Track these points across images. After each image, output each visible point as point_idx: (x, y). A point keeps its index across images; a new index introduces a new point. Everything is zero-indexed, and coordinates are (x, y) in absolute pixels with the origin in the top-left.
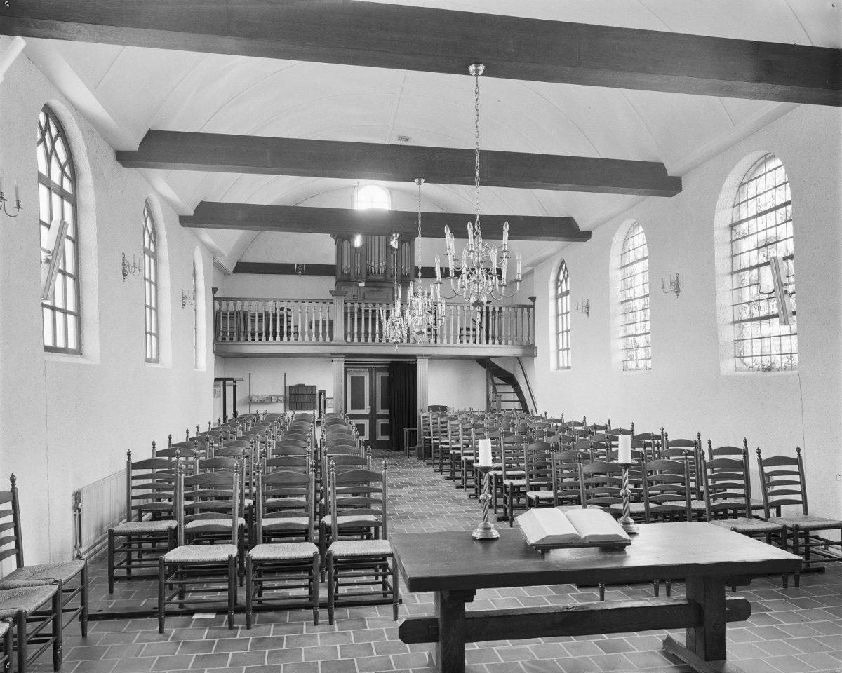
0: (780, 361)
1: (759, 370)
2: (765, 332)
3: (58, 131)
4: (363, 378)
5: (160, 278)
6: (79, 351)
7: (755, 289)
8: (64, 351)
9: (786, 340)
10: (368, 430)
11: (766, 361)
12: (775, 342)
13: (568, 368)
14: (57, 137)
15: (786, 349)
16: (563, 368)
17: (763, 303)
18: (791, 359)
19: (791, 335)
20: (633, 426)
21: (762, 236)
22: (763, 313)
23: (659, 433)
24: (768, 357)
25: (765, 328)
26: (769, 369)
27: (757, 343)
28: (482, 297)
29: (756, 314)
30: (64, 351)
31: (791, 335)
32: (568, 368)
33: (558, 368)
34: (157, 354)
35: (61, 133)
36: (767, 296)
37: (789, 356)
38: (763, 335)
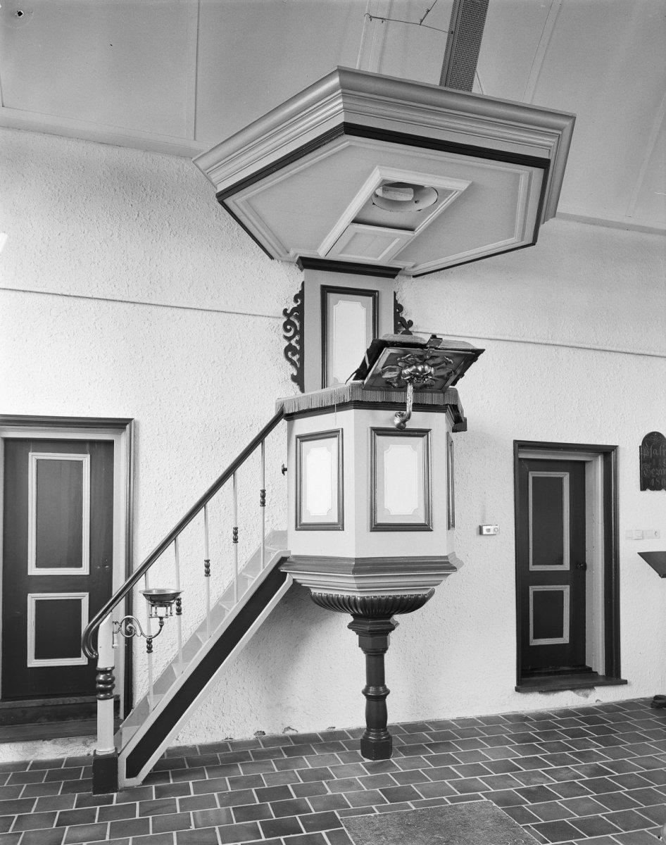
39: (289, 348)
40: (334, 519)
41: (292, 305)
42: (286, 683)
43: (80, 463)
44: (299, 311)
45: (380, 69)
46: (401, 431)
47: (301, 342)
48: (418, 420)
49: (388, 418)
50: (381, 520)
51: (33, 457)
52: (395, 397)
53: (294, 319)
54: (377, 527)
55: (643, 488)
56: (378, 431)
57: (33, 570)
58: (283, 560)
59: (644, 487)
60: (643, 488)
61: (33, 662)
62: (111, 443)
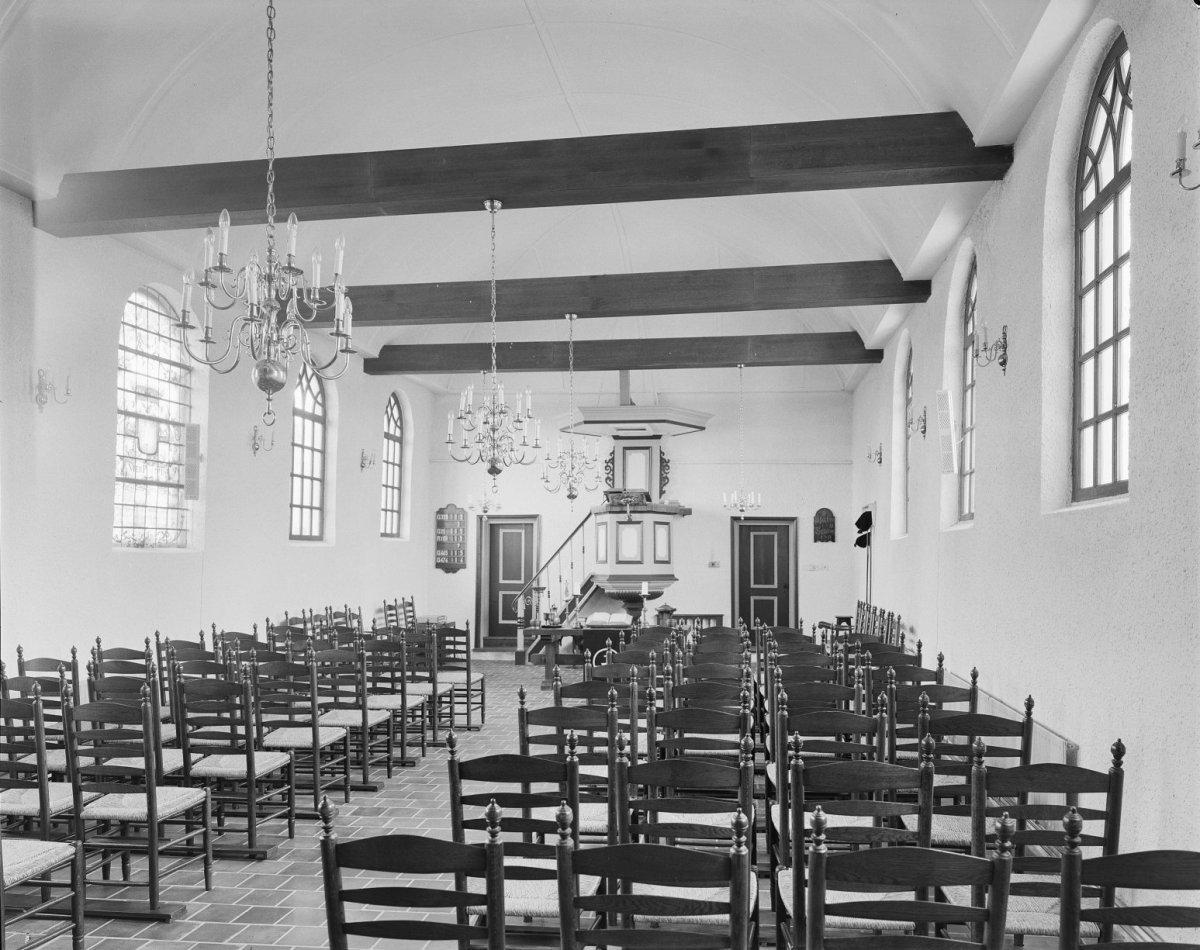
0: (154, 536)
1: (129, 546)
2: (140, 500)
3: (1081, 363)
4: (773, 536)
5: (902, 495)
6: (398, 535)
7: (130, 442)
8: (310, 538)
9: (162, 514)
10: (408, 910)
11: (138, 534)
12: (150, 513)
13: (1118, 488)
14: (1088, 355)
15: (162, 523)
16: (1101, 491)
17: (140, 464)
18: (166, 535)
19: (168, 508)
20: (255, 628)
21: (143, 382)
22: (140, 476)
23: (343, 610)
24: (142, 531)
25: (140, 494)
26: (142, 545)
27: (129, 512)
28: (271, 372)
29: (131, 475)
30: (310, 538)
31: (168, 508)
32: (1118, 488)
33: (1077, 494)
34: (399, 528)
35: (1078, 360)
36: (144, 457)
37: (164, 531)
38: (138, 502)
39: (608, 478)
40: (667, 559)
41: (609, 458)
42: (539, 590)
43: (520, 534)
44: (612, 461)
45: (625, 385)
46: (630, 522)
47: (613, 475)
48: (636, 517)
49: (623, 517)
50: (620, 559)
51: (502, 532)
52: (624, 509)
53: (611, 462)
54: (619, 562)
55: (815, 541)
56: (620, 523)
57: (501, 581)
58: (592, 576)
59: (817, 539)
60: (815, 541)
61: (501, 621)
62: (532, 524)
